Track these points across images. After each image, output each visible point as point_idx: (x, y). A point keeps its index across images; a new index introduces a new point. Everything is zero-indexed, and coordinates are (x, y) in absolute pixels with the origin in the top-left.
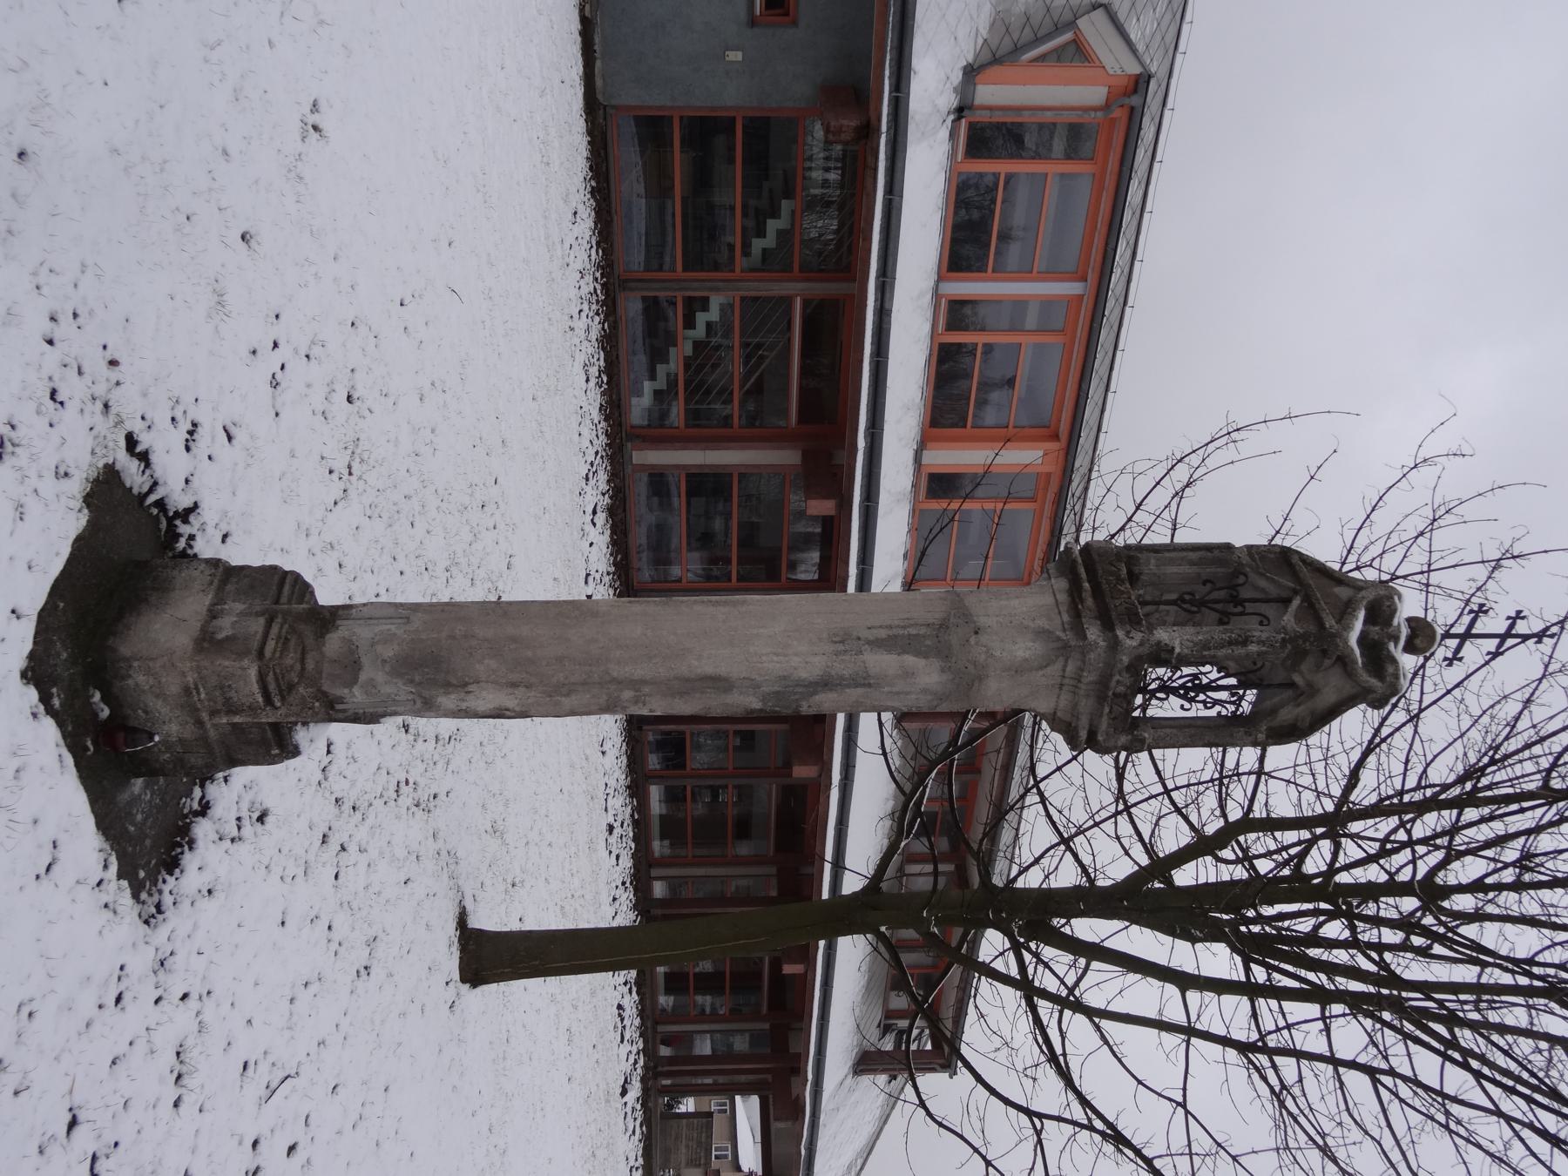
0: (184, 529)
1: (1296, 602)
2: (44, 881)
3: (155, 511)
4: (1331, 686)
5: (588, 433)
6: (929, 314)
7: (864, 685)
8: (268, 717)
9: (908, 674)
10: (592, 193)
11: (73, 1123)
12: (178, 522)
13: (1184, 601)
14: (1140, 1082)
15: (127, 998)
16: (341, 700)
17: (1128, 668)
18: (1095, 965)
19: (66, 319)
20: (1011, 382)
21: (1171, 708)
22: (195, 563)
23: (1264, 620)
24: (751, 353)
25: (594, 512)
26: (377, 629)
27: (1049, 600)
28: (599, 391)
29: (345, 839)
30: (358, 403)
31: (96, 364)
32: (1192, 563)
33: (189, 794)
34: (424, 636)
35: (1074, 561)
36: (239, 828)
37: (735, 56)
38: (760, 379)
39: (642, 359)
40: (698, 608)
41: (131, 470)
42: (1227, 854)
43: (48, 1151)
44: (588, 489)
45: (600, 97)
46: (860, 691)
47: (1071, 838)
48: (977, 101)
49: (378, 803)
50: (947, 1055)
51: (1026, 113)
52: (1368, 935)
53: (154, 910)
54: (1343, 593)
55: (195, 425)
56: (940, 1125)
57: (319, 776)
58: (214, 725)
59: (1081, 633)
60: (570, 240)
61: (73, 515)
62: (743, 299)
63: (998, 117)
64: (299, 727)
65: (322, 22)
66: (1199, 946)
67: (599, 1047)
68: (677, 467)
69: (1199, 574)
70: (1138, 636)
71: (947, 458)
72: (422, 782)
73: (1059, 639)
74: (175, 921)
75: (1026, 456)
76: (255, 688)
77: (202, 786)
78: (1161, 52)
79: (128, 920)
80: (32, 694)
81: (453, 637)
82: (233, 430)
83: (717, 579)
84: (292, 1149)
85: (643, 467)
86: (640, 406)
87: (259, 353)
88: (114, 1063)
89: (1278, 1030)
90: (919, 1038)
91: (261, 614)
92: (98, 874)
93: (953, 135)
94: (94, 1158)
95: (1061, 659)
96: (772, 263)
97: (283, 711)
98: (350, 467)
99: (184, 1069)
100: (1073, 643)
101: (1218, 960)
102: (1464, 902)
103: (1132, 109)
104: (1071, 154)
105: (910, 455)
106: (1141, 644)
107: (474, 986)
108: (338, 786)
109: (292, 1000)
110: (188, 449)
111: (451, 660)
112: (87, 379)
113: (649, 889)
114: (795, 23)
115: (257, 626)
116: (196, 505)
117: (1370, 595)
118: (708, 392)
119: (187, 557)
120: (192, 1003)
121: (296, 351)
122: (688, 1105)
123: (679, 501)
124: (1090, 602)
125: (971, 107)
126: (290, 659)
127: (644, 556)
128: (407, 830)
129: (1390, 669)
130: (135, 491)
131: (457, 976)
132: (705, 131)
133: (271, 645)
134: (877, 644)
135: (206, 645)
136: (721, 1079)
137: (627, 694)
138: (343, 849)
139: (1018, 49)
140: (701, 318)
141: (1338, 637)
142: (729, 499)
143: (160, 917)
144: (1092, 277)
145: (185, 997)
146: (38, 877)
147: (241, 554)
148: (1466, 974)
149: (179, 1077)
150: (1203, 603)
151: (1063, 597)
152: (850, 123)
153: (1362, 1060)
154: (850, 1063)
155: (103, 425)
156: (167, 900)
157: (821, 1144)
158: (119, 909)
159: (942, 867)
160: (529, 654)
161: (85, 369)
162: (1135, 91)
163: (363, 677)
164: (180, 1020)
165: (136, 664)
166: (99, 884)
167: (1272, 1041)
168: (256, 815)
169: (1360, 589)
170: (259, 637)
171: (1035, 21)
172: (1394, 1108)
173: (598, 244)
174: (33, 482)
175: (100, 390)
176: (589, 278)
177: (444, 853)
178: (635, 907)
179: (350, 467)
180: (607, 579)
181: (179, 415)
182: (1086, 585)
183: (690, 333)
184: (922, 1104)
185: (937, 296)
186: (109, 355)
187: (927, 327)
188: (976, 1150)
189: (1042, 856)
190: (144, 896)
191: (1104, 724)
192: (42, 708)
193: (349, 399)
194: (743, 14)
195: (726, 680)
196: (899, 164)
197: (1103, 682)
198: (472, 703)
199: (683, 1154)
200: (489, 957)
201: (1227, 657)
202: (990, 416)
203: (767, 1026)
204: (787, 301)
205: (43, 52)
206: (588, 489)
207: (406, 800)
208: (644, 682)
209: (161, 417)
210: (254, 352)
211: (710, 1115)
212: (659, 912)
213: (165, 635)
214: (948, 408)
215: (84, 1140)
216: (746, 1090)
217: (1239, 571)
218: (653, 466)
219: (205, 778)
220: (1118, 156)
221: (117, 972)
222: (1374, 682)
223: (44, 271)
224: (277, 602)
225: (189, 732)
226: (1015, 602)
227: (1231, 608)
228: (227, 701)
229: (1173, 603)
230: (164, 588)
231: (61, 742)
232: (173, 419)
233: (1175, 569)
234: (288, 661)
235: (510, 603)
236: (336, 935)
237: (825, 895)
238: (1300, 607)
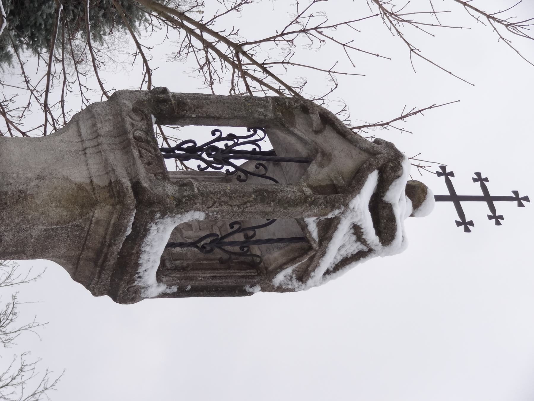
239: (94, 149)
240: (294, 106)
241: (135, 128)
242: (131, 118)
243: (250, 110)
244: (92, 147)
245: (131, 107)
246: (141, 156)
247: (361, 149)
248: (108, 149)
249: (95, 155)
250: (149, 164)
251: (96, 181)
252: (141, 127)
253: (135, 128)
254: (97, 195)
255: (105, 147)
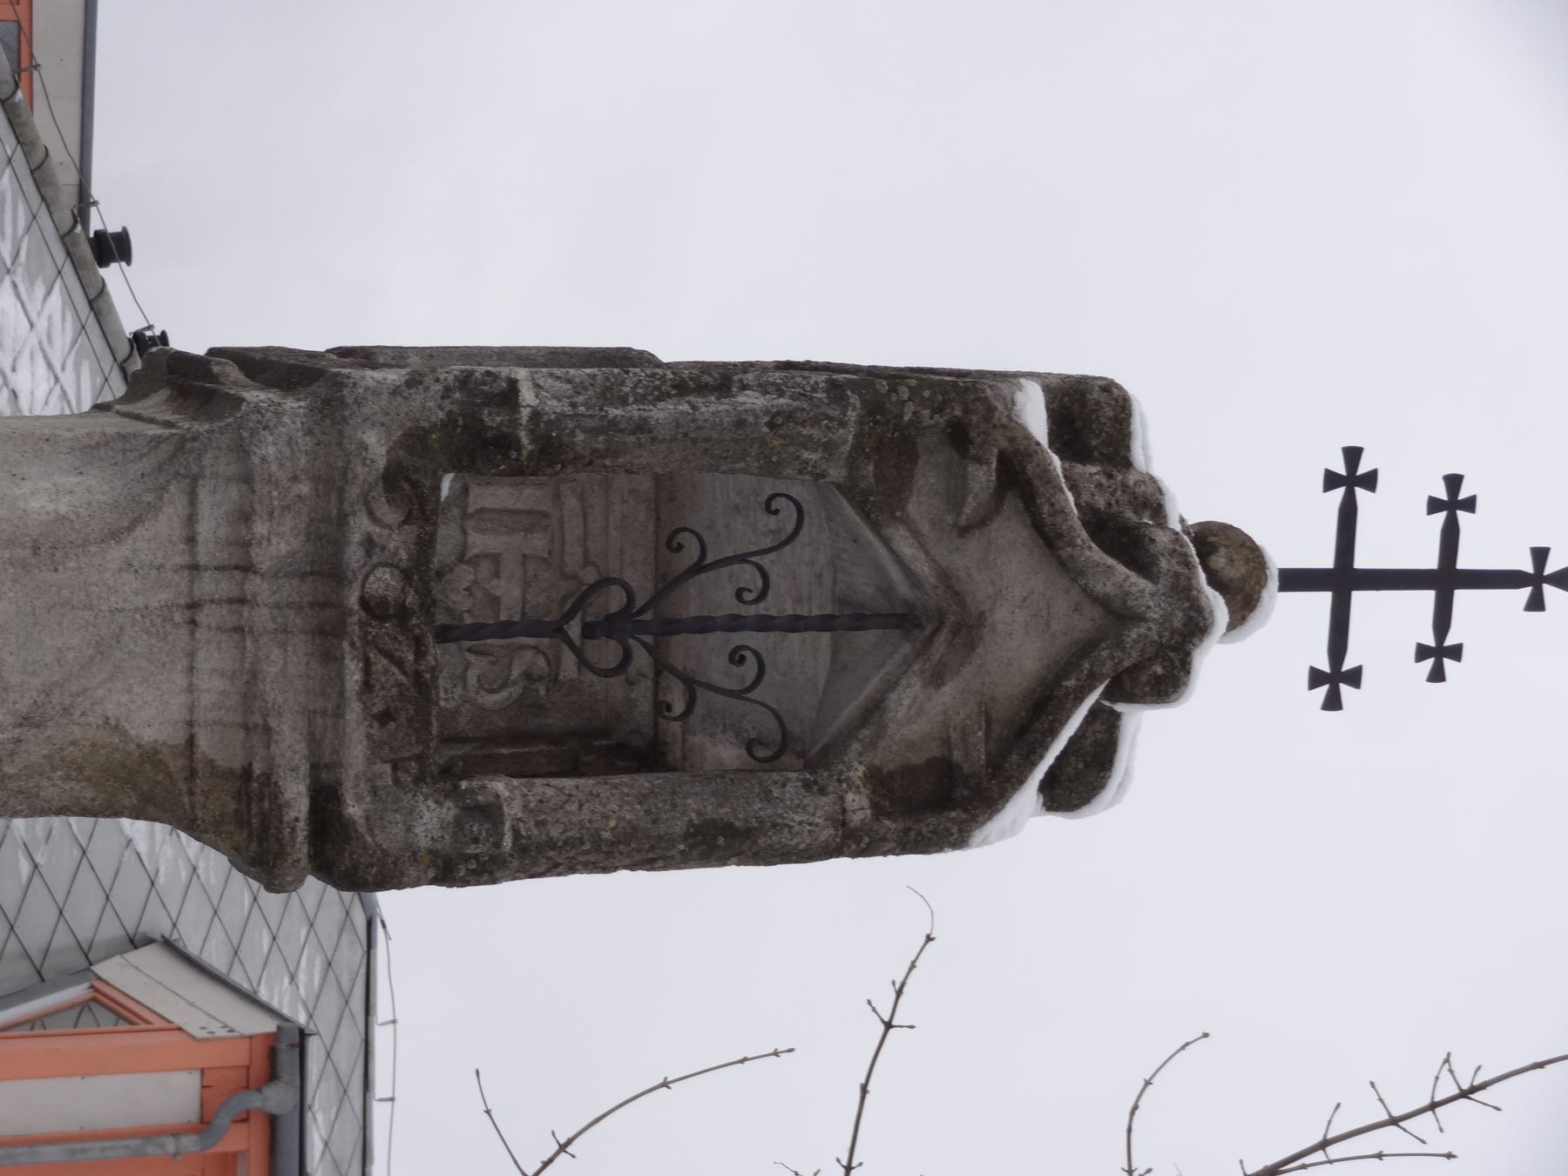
95: (176, 492)
103: (273, 1121)
162: (272, 1075)
197: (324, 565)
239: (225, 610)
240: (927, 422)
241: (375, 559)
242: (371, 515)
243: (774, 459)
244: (219, 602)
245: (382, 463)
246: (367, 686)
247: (1086, 591)
248: (271, 626)
249: (224, 637)
250: (385, 717)
251: (205, 743)
252: (396, 554)
253: (375, 559)
254: (199, 798)
255: (261, 617)
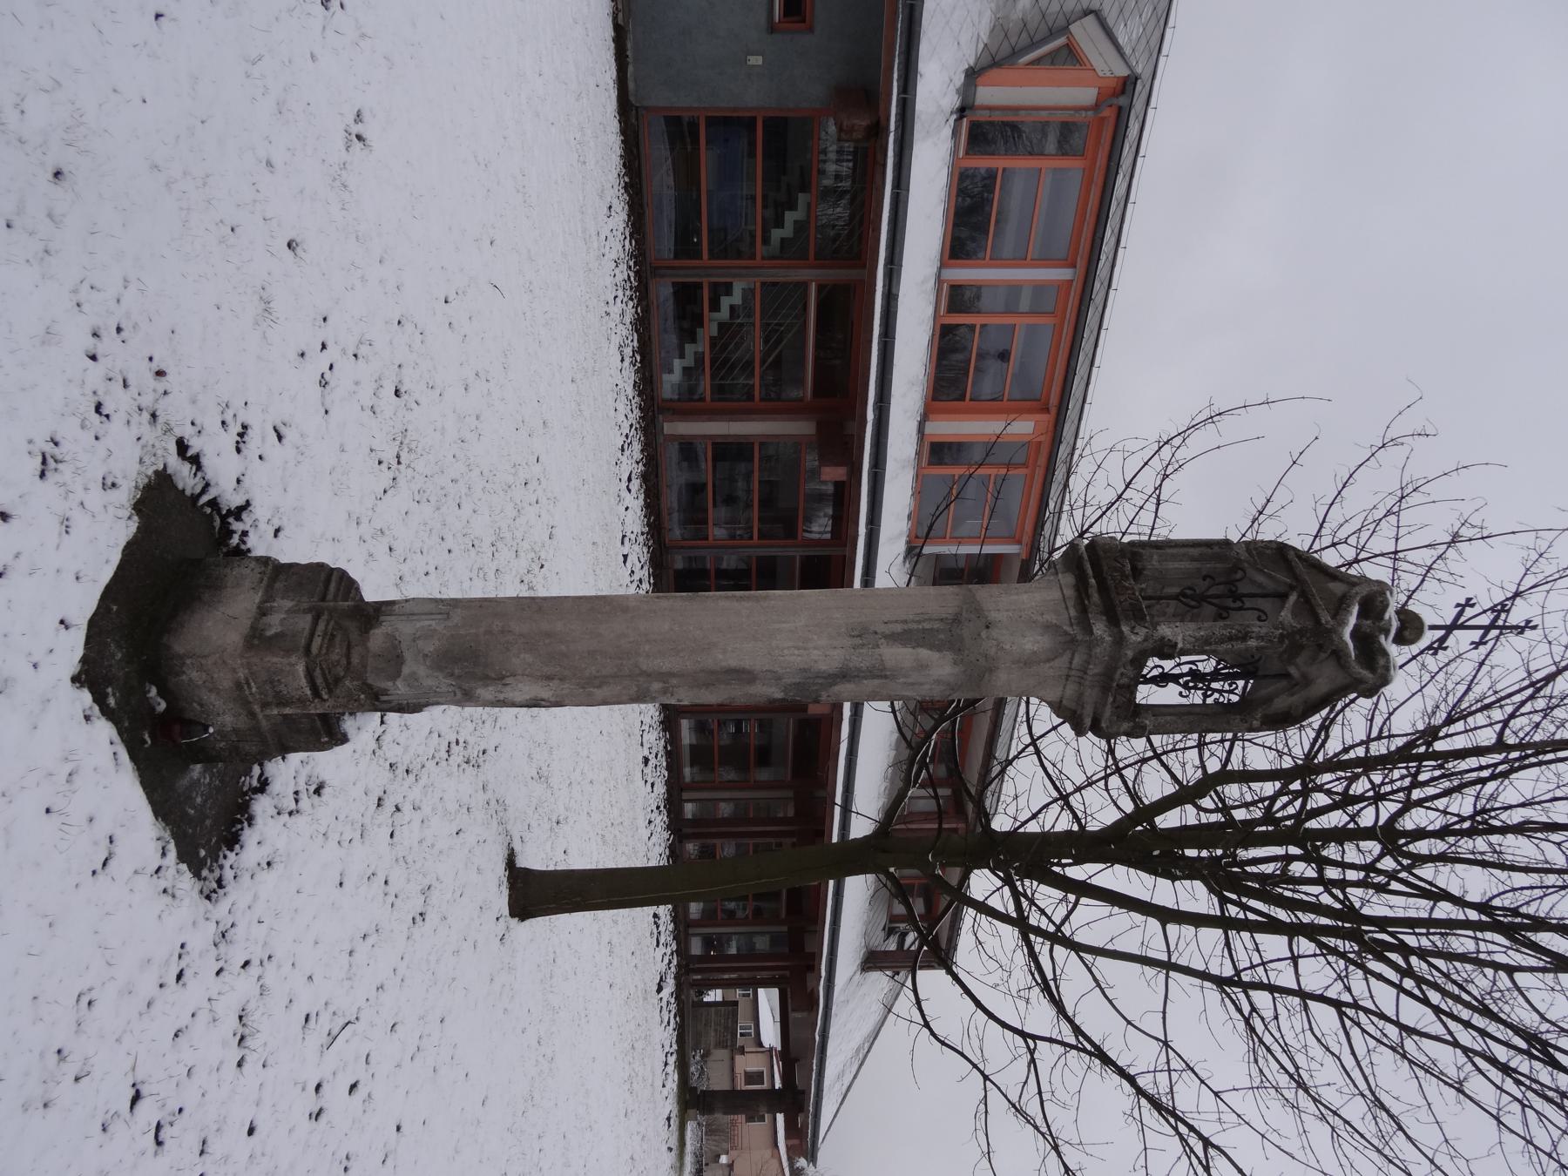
0: (237, 526)
1: (1293, 598)
2: (101, 876)
3: (208, 510)
4: (1324, 677)
5: (623, 408)
6: (932, 298)
7: (880, 677)
8: (316, 708)
9: (922, 667)
10: (625, 188)
11: (136, 1098)
12: (231, 520)
13: (1185, 596)
14: (1129, 1023)
15: (188, 974)
16: (385, 692)
17: (1132, 661)
18: (1083, 900)
19: (109, 334)
20: (1004, 356)
21: (1170, 695)
22: (246, 562)
23: (1262, 616)
24: (772, 336)
25: (630, 479)
26: (418, 625)
27: (1057, 595)
28: (633, 369)
29: (399, 800)
30: (405, 397)
31: (141, 375)
32: (1193, 559)
33: (248, 772)
34: (462, 632)
35: (1081, 557)
36: (297, 801)
37: (755, 60)
38: (779, 356)
39: (672, 339)
40: (722, 603)
41: (183, 474)
42: (1207, 802)
43: (111, 1129)
44: (624, 459)
45: (632, 99)
46: (876, 682)
47: (1069, 795)
48: (978, 102)
49: (431, 765)
50: (941, 956)
51: (1022, 113)
52: (1332, 873)
53: (215, 885)
54: (1337, 588)
55: (245, 427)
56: (943, 1043)
57: (374, 745)
58: (266, 717)
59: (1089, 630)
60: (605, 232)
61: (122, 523)
62: (763, 284)
63: (998, 117)
64: (346, 717)
65: (363, 36)
66: (1177, 883)
67: (637, 953)
68: (704, 437)
69: (1199, 570)
70: (1143, 632)
71: (948, 428)
72: (471, 740)
73: (1066, 633)
74: (237, 894)
75: (1024, 427)
76: (303, 682)
77: (261, 765)
78: (1146, 55)
79: (187, 902)
80: (86, 696)
81: (489, 632)
82: (283, 430)
83: (741, 537)
84: (353, 1087)
85: (673, 438)
86: (671, 382)
87: (307, 356)
88: (176, 1035)
89: (1253, 967)
90: (921, 939)
91: (309, 610)
92: (156, 861)
93: (955, 133)
94: (159, 1127)
96: (791, 250)
97: (330, 703)
98: (398, 457)
99: (247, 1031)
100: (1079, 637)
101: (1195, 896)
102: (1422, 847)
103: (1120, 108)
104: (1064, 149)
105: (914, 426)
106: (1145, 640)
107: (522, 919)
108: (391, 752)
109: (351, 953)
110: (238, 450)
111: (493, 652)
112: (133, 390)
113: (681, 810)
114: (811, 30)
115: (304, 622)
116: (248, 504)
117: (1363, 591)
118: (733, 367)
119: (240, 553)
120: (254, 970)
121: (344, 351)
122: (714, 995)
123: (706, 465)
124: (1095, 597)
125: (972, 107)
126: (337, 654)
127: (676, 516)
128: (456, 785)
129: (1382, 662)
130: (188, 493)
131: (506, 911)
132: (730, 126)
133: (317, 641)
134: (893, 638)
135: (256, 642)
136: (745, 975)
137: (656, 686)
138: (398, 809)
139: (1015, 53)
140: (726, 302)
141: (1334, 631)
142: (751, 459)
143: (221, 892)
144: (1081, 263)
145: (247, 963)
146: (94, 873)
147: (293, 551)
148: (1419, 908)
149: (242, 1038)
150: (1202, 599)
151: (1070, 592)
152: (862, 122)
153: (1332, 994)
154: (858, 962)
155: (150, 434)
156: (228, 874)
157: (832, 1031)
158: (178, 893)
159: (941, 792)
160: (563, 647)
161: (130, 382)
162: (1123, 92)
163: (406, 670)
164: (242, 987)
165: (188, 661)
166: (157, 871)
167: (1246, 977)
168: (312, 788)
169: (1354, 584)
170: (306, 633)
171: (1032, 26)
172: (1355, 1032)
173: (631, 235)
174: (80, 494)
175: (147, 401)
176: (623, 267)
177: (493, 802)
178: (669, 828)
179: (398, 457)
180: (641, 539)
181: (228, 418)
182: (1093, 581)
183: (716, 315)
184: (927, 1025)
185: (939, 281)
186: (155, 366)
187: (930, 310)
188: (975, 1066)
189: (1039, 812)
190: (205, 873)
191: (1108, 712)
192: (96, 708)
193: (397, 393)
194: (763, 20)
195: (749, 672)
196: (905, 161)
197: (1108, 674)
198: (509, 694)
199: (712, 1037)
200: (535, 894)
201: (1226, 652)
202: (987, 387)
203: (785, 929)
204: (803, 286)
205: (77, 71)
206: (624, 459)
207: (457, 758)
208: (672, 675)
209: (211, 422)
210: (302, 355)
211: (736, 1003)
212: (690, 831)
213: (217, 633)
214: (949, 382)
215: (148, 1112)
216: (766, 984)
217: (1237, 566)
218: (682, 436)
219: (262, 757)
220: (1106, 153)
221: (178, 950)
222: (1366, 674)
223: (85, 287)
224: (323, 599)
225: (243, 722)
226: (1025, 597)
227: (1229, 603)
228: (278, 694)
229: (1176, 597)
230: (216, 586)
231: (117, 739)
232: (223, 423)
233: (1176, 565)
234: (334, 657)
235: (545, 599)
236: (392, 889)
237: (835, 839)
238: (1296, 602)
